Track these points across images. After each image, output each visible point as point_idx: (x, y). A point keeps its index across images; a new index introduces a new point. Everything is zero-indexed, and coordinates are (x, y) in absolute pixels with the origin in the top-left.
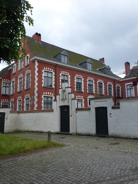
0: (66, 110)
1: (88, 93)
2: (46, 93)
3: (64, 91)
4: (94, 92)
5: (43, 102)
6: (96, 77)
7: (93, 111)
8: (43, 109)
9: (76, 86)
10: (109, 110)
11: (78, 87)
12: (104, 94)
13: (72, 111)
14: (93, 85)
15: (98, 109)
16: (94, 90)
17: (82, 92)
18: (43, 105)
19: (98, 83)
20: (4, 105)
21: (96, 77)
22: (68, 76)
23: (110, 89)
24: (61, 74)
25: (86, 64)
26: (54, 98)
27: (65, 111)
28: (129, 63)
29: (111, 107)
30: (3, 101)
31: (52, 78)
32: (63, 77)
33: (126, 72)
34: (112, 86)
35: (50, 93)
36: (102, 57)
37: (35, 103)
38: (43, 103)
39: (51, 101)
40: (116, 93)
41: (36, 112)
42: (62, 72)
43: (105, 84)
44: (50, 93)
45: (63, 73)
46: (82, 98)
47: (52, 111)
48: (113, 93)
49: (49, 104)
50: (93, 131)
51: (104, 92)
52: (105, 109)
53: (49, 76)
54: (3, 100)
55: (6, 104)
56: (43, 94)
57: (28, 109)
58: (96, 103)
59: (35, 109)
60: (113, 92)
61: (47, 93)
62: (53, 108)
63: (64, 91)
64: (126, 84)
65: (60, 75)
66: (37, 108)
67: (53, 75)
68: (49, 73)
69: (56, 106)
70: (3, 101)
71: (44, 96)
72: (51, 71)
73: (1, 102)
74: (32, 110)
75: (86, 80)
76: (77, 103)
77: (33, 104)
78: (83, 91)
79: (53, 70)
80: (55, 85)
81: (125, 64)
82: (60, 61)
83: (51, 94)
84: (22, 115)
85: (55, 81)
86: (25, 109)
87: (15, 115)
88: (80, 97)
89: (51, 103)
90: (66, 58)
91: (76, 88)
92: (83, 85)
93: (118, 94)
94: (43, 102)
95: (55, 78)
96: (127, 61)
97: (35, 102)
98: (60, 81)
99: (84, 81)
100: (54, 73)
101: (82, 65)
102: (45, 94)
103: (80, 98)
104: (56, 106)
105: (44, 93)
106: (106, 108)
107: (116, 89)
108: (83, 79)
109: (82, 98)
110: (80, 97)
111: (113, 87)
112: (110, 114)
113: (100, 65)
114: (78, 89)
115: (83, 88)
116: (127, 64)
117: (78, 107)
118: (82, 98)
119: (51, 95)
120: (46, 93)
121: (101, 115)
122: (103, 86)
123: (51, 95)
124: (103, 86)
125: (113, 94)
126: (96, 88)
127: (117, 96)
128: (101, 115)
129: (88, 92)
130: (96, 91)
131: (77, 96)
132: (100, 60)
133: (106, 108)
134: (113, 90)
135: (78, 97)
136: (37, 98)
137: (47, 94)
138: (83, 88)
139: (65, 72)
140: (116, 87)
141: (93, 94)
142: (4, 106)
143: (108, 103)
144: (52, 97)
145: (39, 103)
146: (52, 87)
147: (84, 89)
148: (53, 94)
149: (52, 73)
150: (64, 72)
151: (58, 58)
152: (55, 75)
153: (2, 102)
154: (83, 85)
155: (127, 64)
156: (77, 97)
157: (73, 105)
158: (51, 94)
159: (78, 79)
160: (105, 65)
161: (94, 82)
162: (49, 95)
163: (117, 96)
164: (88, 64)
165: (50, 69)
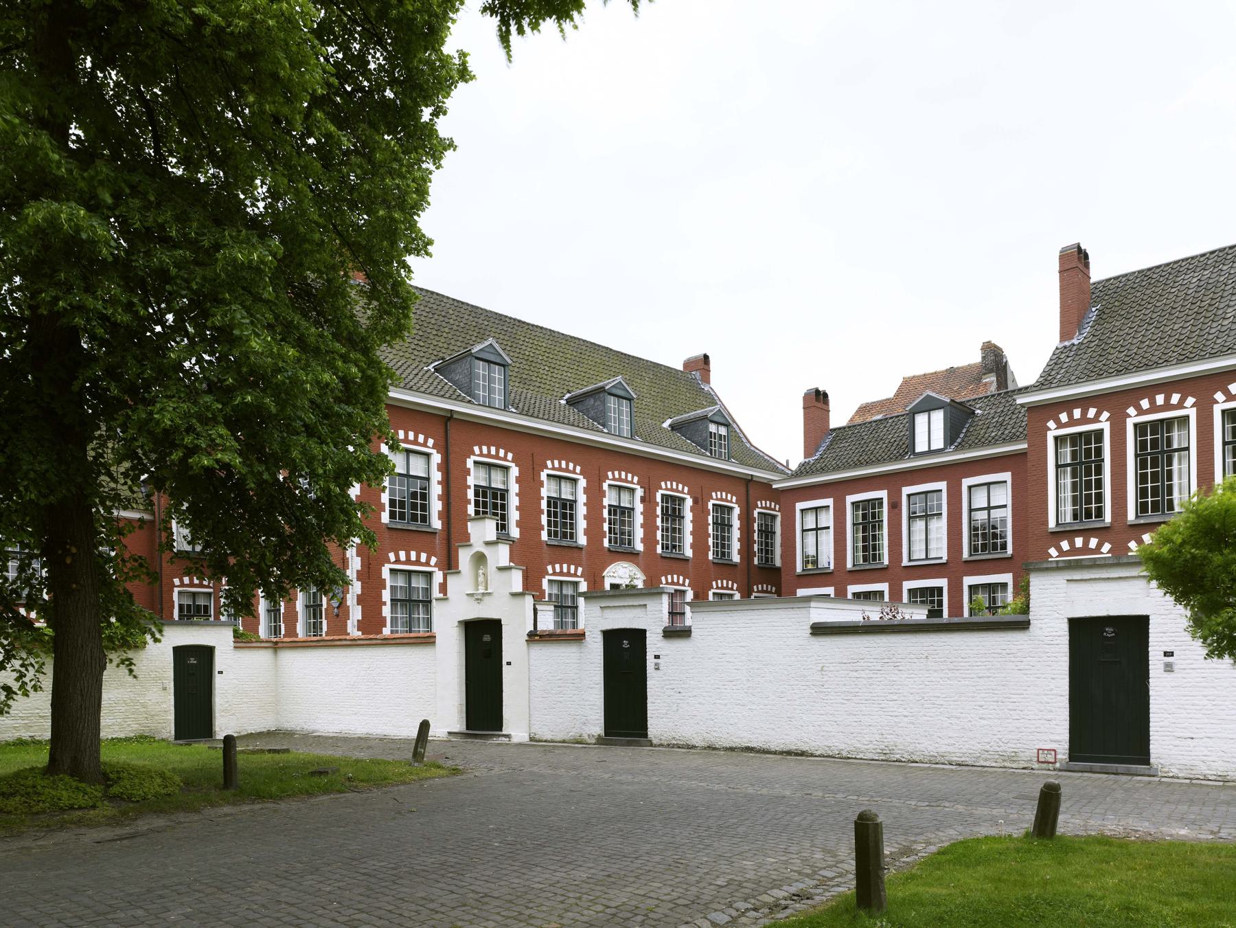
0: (487, 638)
1: (609, 550)
2: (402, 555)
3: (480, 559)
4: (639, 547)
5: (386, 595)
6: (652, 469)
7: (595, 648)
8: (386, 631)
9: (549, 515)
10: (654, 643)
11: (556, 523)
12: (689, 553)
13: (513, 645)
14: (633, 509)
15: (612, 638)
16: (639, 533)
17: (580, 548)
18: (386, 611)
19: (659, 499)
20: (189, 606)
21: (652, 469)
22: (506, 469)
23: (723, 526)
24: (473, 458)
25: (604, 402)
26: (438, 577)
27: (482, 640)
28: (825, 395)
29: (660, 630)
30: (182, 585)
31: (428, 479)
32: (482, 473)
33: (811, 445)
34: (737, 511)
35: (418, 556)
36: (698, 352)
37: (349, 603)
38: (389, 603)
39: (428, 591)
40: (756, 547)
41: (354, 644)
42: (476, 449)
43: (695, 501)
44: (418, 556)
45: (481, 455)
46: (579, 573)
47: (429, 640)
48: (736, 545)
49: (415, 604)
50: (596, 727)
51: (692, 546)
52: (638, 637)
53: (412, 473)
54: (181, 581)
55: (201, 602)
56: (389, 562)
57: (316, 627)
58: (608, 613)
59: (353, 631)
60: (739, 540)
61: (408, 556)
62: (436, 628)
63: (480, 559)
64: (800, 506)
65: (470, 463)
66: (361, 626)
67: (434, 467)
68: (413, 458)
69: (447, 622)
70: (182, 585)
71: (391, 570)
72: (425, 445)
73: (176, 590)
74: (336, 637)
75: (601, 487)
76: (535, 611)
77: (342, 604)
78: (582, 540)
79: (431, 442)
80: (446, 515)
81: (807, 397)
82: (468, 391)
83: (424, 557)
84: (293, 660)
85: (446, 497)
86: (300, 628)
87: (258, 659)
88: (569, 569)
89: (427, 603)
90: (498, 374)
91: (549, 525)
92: (581, 510)
93: (767, 550)
94: (386, 595)
95: (446, 483)
96: (813, 386)
97: (349, 596)
98: (471, 494)
99: (586, 491)
100: (436, 458)
101: (580, 407)
102: (398, 561)
103: (568, 574)
104: (447, 622)
105: (392, 556)
106: (642, 633)
107: (756, 528)
108: (582, 483)
109: (579, 573)
110: (565, 570)
111: (740, 518)
112: (657, 657)
113: (683, 395)
114: (556, 532)
115: (582, 524)
116: (817, 400)
117: (540, 627)
118: (575, 575)
119: (427, 564)
120: (402, 555)
121: (625, 660)
122: (688, 516)
123: (427, 564)
124: (688, 516)
125: (740, 552)
126: (649, 526)
127: (756, 562)
128: (625, 660)
129: (606, 543)
130: (649, 539)
131: (554, 569)
132: (689, 364)
133: (642, 633)
134: (736, 534)
135: (558, 570)
136: (358, 579)
137: (408, 562)
138: (582, 524)
139: (493, 449)
140: (756, 515)
141: (631, 556)
142: (189, 610)
143: (651, 617)
144: (429, 575)
145: (370, 600)
146: (429, 526)
147: (586, 532)
148: (434, 560)
149: (428, 455)
150: (489, 451)
151: (460, 373)
152: (445, 467)
153: (180, 593)
154: (581, 510)
155: (817, 400)
156: (550, 571)
157: (517, 620)
158: (424, 557)
159: (561, 481)
160: (712, 399)
161: (639, 492)
162: (418, 562)
163: (756, 562)
164: (612, 402)
165: (416, 437)
